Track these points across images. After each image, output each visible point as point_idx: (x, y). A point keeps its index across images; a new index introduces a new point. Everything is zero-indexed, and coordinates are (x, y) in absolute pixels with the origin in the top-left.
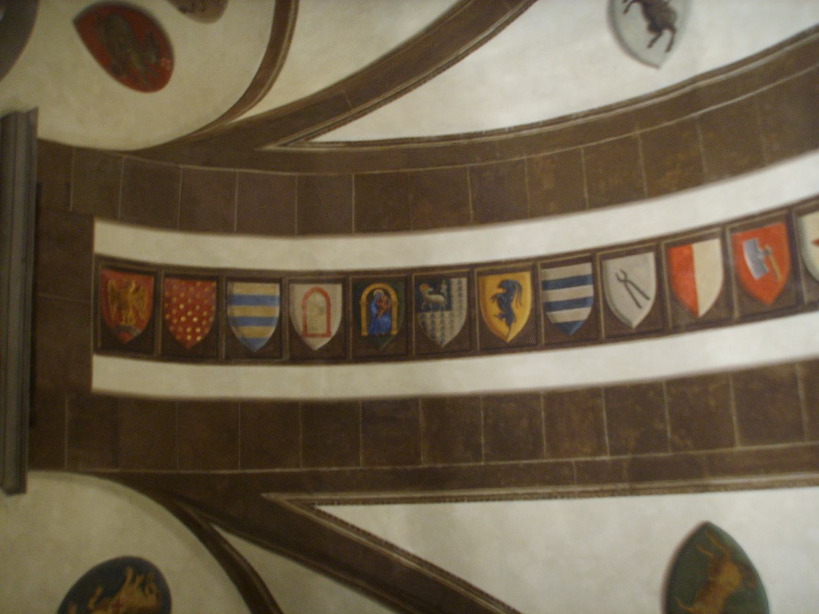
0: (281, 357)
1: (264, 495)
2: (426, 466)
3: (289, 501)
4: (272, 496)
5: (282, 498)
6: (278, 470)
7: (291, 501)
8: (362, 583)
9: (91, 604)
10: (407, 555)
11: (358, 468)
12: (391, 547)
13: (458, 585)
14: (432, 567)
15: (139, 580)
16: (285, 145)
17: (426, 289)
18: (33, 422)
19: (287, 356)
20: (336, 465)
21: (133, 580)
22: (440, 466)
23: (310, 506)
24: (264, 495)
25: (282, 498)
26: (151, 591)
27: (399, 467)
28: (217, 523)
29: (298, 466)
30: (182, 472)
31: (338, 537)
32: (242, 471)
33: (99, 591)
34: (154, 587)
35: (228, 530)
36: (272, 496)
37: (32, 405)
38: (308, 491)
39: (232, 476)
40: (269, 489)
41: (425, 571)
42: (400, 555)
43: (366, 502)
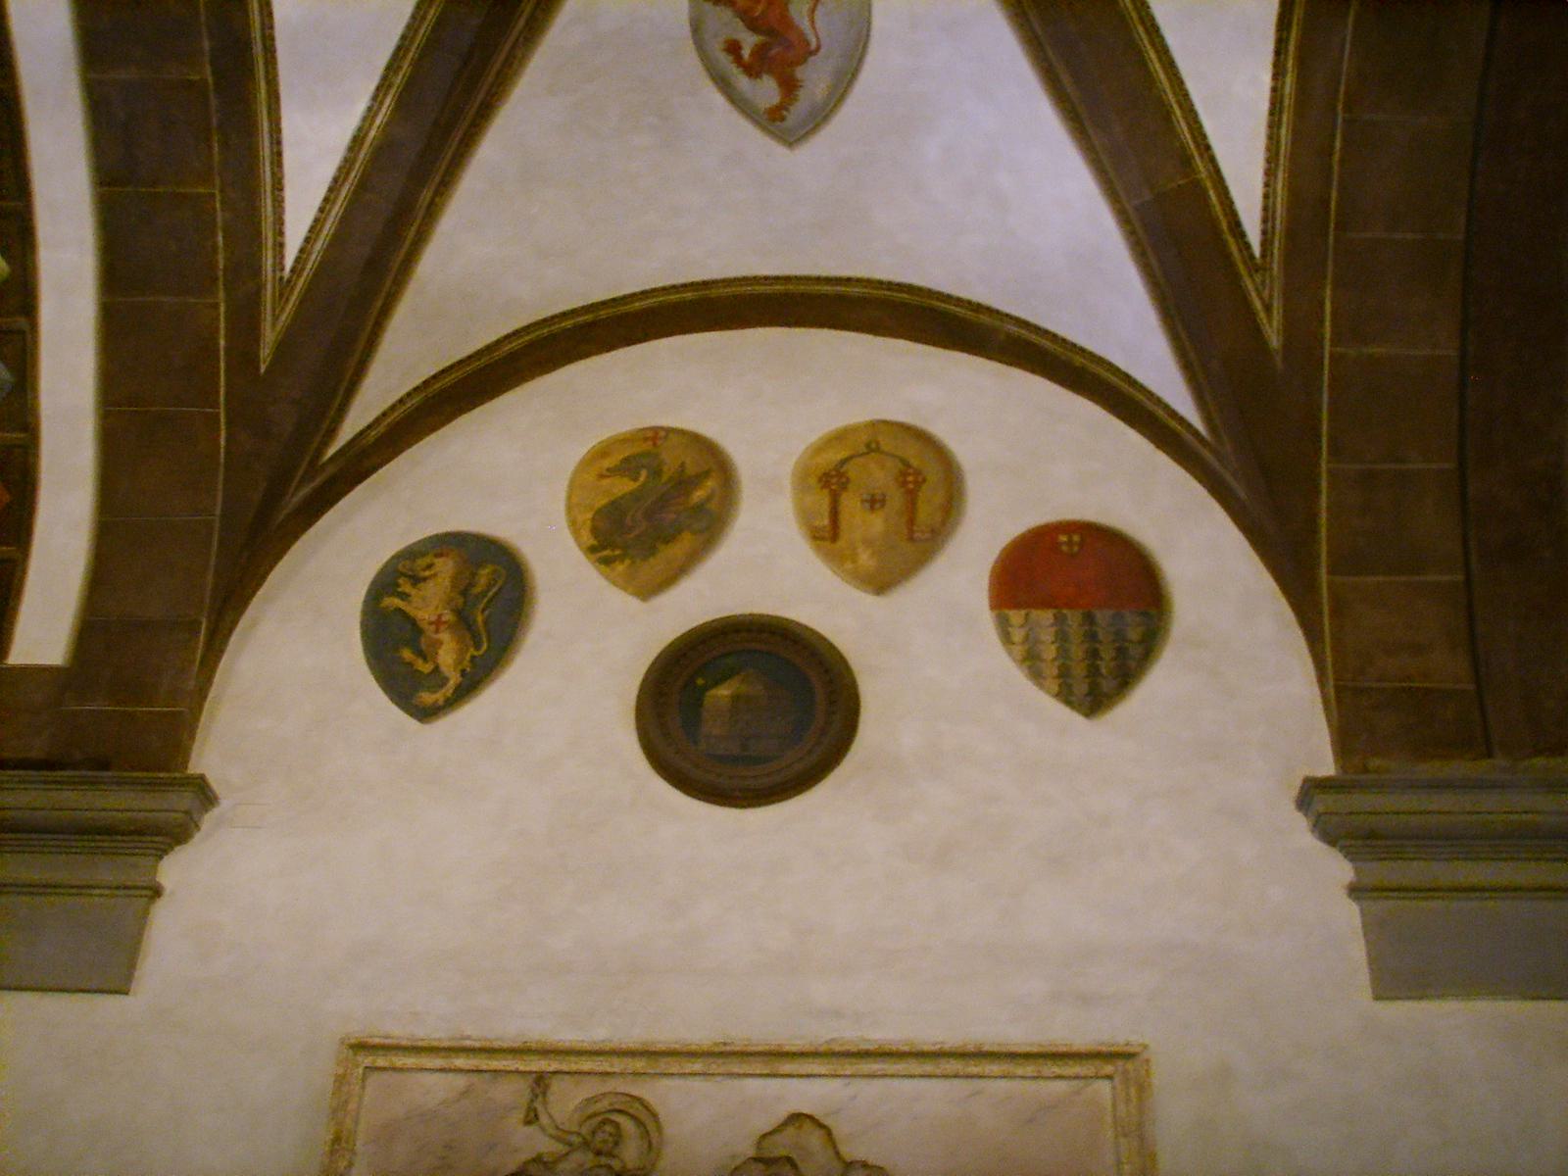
0: (21, 333)
1: (263, 368)
2: (208, 70)
3: (274, 325)
4: (266, 353)
5: (269, 336)
6: (222, 342)
7: (276, 318)
8: (426, 195)
9: (425, 668)
10: (370, 114)
11: (218, 197)
12: (357, 140)
13: (424, 18)
14: (392, 68)
15: (406, 588)
16: (276, 318)
17: (746, 53)
18: (104, 765)
19: (21, 322)
20: (214, 235)
21: (404, 596)
22: (206, 44)
23: (285, 287)
24: (263, 368)
25: (269, 336)
26: (430, 566)
27: (214, 121)
28: (319, 452)
29: (216, 306)
30: (218, 512)
31: (338, 241)
32: (222, 406)
33: (407, 654)
34: (422, 562)
35: (332, 433)
36: (266, 353)
37: (74, 766)
38: (259, 290)
39: (229, 422)
40: (253, 361)
41: (398, 80)
42: (371, 125)
43: (278, 186)
